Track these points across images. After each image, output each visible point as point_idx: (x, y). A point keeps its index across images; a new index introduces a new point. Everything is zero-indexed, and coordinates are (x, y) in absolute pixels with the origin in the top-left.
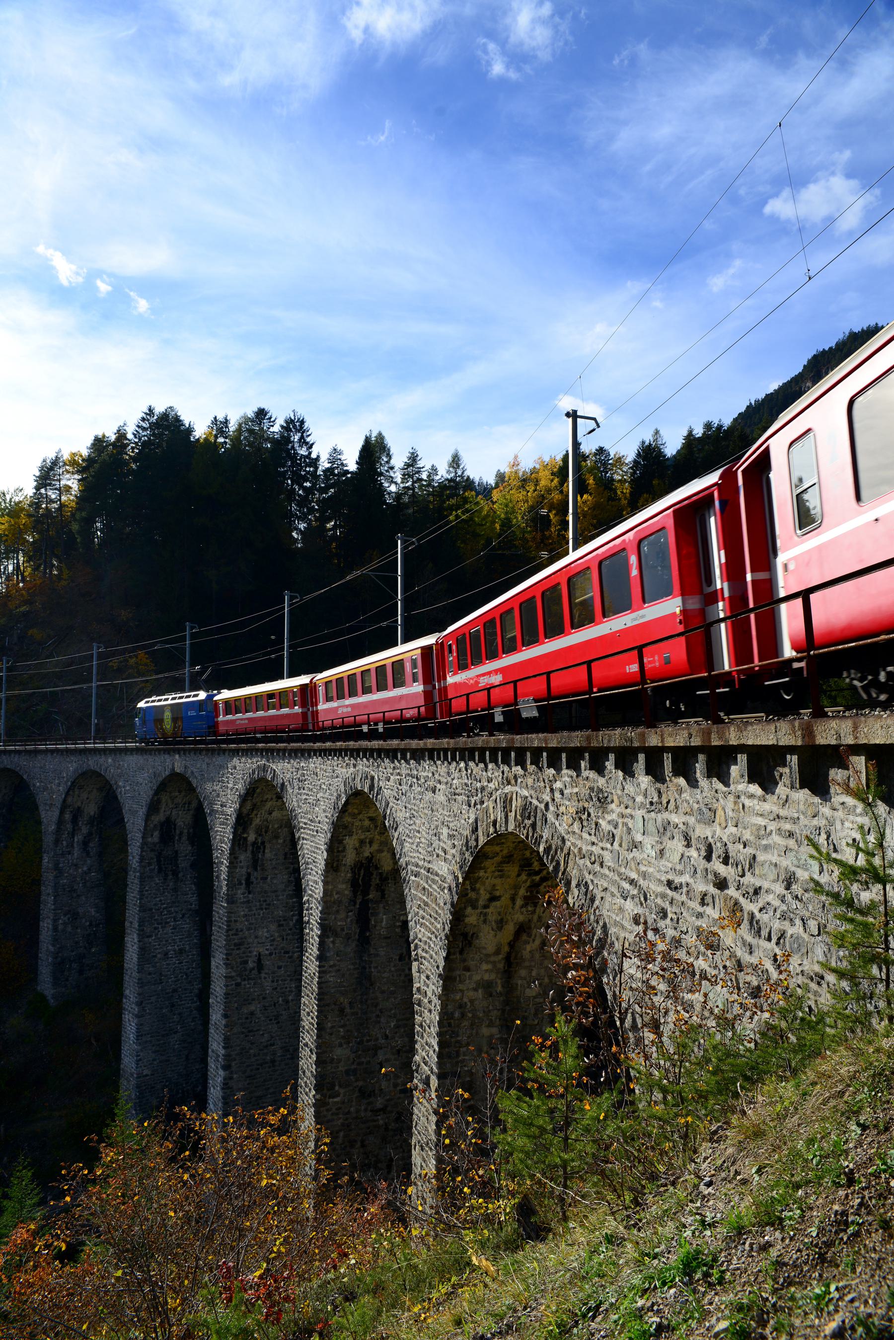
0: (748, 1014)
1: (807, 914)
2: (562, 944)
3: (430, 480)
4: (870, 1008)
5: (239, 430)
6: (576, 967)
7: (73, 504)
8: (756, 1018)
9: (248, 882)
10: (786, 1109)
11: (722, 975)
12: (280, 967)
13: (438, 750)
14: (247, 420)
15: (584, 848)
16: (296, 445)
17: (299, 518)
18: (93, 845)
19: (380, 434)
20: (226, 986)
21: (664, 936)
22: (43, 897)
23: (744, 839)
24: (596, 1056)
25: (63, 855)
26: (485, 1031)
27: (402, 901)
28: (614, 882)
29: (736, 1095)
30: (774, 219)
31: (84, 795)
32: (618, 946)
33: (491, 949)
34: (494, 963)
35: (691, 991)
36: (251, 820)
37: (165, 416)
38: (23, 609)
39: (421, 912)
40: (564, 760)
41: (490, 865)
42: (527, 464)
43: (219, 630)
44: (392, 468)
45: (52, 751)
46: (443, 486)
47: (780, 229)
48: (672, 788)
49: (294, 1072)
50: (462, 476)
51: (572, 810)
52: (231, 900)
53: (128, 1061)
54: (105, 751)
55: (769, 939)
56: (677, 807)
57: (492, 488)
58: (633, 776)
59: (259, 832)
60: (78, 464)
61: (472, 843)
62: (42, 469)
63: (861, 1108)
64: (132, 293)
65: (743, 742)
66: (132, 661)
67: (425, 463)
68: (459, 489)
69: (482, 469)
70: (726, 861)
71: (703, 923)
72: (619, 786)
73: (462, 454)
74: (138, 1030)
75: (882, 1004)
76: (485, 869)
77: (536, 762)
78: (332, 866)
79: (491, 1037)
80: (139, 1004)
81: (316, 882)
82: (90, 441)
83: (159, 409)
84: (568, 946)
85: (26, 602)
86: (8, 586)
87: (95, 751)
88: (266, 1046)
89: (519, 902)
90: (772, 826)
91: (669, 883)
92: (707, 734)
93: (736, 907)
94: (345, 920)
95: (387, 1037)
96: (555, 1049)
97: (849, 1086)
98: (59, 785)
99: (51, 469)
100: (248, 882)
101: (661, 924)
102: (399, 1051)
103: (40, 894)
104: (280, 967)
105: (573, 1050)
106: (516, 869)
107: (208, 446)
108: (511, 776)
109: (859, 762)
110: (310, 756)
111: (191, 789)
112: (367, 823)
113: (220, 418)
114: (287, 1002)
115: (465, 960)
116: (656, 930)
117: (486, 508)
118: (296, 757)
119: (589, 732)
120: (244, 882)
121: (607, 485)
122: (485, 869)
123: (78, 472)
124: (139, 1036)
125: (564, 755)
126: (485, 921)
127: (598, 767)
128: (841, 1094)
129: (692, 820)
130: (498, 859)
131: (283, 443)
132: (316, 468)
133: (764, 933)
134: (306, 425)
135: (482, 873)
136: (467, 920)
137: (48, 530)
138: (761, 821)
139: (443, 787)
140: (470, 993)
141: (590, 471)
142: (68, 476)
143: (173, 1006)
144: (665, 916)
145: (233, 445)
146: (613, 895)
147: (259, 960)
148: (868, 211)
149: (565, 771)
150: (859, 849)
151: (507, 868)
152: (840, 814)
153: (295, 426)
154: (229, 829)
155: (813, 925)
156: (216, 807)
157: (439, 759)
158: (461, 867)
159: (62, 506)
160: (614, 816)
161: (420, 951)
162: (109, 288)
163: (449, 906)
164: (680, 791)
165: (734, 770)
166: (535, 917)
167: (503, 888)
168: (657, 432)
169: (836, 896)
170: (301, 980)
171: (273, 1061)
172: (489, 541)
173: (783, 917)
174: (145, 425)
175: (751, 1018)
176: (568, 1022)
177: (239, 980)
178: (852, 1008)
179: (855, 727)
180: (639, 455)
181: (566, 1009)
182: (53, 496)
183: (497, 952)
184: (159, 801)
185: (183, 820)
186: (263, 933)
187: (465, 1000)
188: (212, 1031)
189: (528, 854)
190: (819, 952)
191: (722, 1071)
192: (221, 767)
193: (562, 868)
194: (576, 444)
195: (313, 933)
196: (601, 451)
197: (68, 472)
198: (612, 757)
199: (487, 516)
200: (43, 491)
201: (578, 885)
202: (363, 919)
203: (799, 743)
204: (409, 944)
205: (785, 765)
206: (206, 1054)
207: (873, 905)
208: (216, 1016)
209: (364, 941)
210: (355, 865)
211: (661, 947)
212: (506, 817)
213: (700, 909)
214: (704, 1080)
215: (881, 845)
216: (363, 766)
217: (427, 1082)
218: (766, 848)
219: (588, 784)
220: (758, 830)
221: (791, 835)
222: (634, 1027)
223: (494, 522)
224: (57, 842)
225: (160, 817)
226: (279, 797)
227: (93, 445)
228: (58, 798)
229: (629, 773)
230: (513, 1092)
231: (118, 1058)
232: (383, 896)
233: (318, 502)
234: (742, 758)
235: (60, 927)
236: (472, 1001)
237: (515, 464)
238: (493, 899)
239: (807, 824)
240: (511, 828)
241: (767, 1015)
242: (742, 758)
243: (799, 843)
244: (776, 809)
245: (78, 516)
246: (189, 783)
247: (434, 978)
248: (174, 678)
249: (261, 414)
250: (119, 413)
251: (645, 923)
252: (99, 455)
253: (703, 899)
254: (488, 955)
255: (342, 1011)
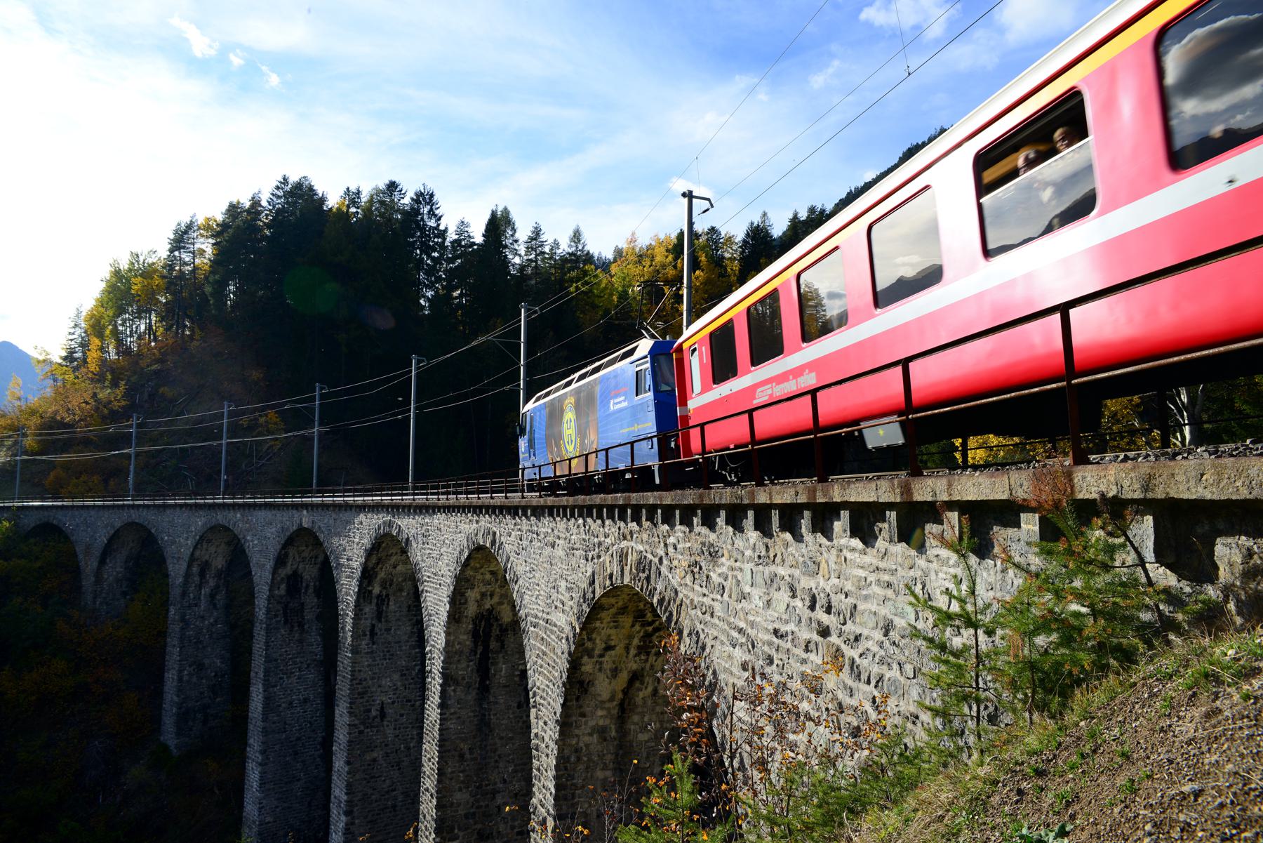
0: (849, 751)
1: (904, 659)
2: (677, 687)
3: (552, 254)
4: (961, 743)
5: (371, 201)
6: (691, 709)
7: (207, 267)
8: (856, 755)
9: (373, 633)
10: (890, 835)
11: (825, 717)
12: (402, 715)
13: (558, 507)
14: (378, 192)
15: (696, 599)
16: (426, 217)
17: (427, 286)
18: (221, 598)
19: (506, 209)
20: (350, 734)
21: (770, 682)
22: (169, 649)
23: (846, 590)
24: (709, 793)
25: (190, 607)
26: (600, 774)
27: (521, 651)
28: (723, 631)
29: (841, 824)
30: (868, 25)
31: (212, 549)
32: (728, 692)
33: (605, 695)
34: (608, 709)
35: (794, 732)
36: (376, 574)
37: (299, 186)
38: (154, 367)
39: (540, 661)
40: (678, 516)
41: (606, 616)
42: (643, 241)
43: (347, 392)
44: (516, 241)
45: (181, 506)
46: (564, 260)
47: (874, 35)
48: (779, 543)
49: (415, 816)
50: (582, 251)
51: (685, 564)
52: (355, 650)
53: (251, 809)
54: (234, 506)
55: (869, 682)
56: (783, 561)
57: (610, 263)
58: (742, 532)
59: (384, 585)
60: (212, 229)
61: (589, 595)
62: (176, 232)
63: (959, 830)
64: (264, 68)
65: (845, 499)
66: (262, 420)
67: (548, 237)
68: (579, 262)
69: (601, 246)
70: (828, 610)
71: (807, 669)
72: (729, 541)
73: (582, 229)
74: (261, 778)
75: (972, 740)
76: (601, 620)
77: (650, 518)
78: (455, 617)
79: (605, 779)
80: (263, 752)
81: (438, 633)
82: (225, 207)
83: (294, 178)
84: (682, 689)
85: (158, 361)
86: (139, 346)
87: (224, 506)
88: (388, 792)
89: (633, 651)
90: (872, 578)
91: (776, 632)
92: (812, 492)
93: (838, 653)
94: (466, 669)
95: (505, 781)
96: (672, 786)
97: (948, 811)
98: (187, 539)
99: (185, 232)
100: (373, 633)
101: (768, 670)
102: (516, 795)
103: (165, 645)
104: (402, 715)
105: (688, 787)
106: (630, 620)
107: (341, 216)
108: (627, 532)
109: (953, 516)
110: (434, 513)
111: (318, 544)
112: (488, 576)
113: (353, 189)
114: (409, 749)
115: (581, 707)
116: (763, 675)
117: (605, 281)
118: (421, 513)
119: (701, 490)
120: (368, 633)
121: (718, 262)
122: (601, 620)
123: (213, 236)
124: (263, 783)
125: (677, 512)
126: (600, 670)
127: (709, 523)
128: (942, 818)
129: (797, 573)
130: (613, 611)
131: (412, 215)
132: (444, 239)
133: (864, 677)
134: (435, 199)
135: (598, 624)
136: (583, 669)
137: (181, 292)
138: (862, 573)
139: (561, 542)
140: (585, 738)
141: (703, 248)
142: (202, 240)
143: (296, 753)
144: (771, 662)
145: (365, 215)
146: (722, 643)
147: (382, 708)
148: (951, 23)
149: (678, 527)
150: (951, 596)
151: (621, 619)
152: (934, 566)
153: (424, 199)
154: (355, 582)
155: (909, 669)
156: (342, 561)
157: (558, 515)
158: (578, 618)
159: (195, 269)
160: (724, 569)
161: (538, 698)
162: (242, 62)
163: (566, 655)
164: (787, 546)
165: (837, 526)
166: (648, 666)
167: (617, 637)
168: (765, 214)
169: (931, 641)
170: (422, 727)
171: (394, 806)
172: (607, 312)
173: (881, 662)
174: (280, 193)
175: (852, 755)
176: (684, 761)
177: (362, 728)
178: (948, 744)
179: (950, 485)
180: (748, 235)
181: (682, 749)
182: (187, 259)
183: (612, 699)
184: (286, 555)
185: (310, 573)
186: (386, 682)
187: (581, 744)
188: (335, 777)
189: (641, 605)
190: (915, 693)
191: (828, 804)
192: (348, 522)
193: (674, 618)
194: (691, 224)
195: (435, 683)
196: (713, 230)
197: (202, 236)
198: (723, 513)
199: (606, 288)
200: (177, 253)
201: (690, 635)
202: (483, 670)
203: (898, 500)
204: (527, 692)
205: (884, 521)
206: (329, 801)
207: (966, 648)
208: (339, 763)
209: (484, 690)
210: (477, 617)
211: (769, 690)
212: (622, 571)
213: (804, 656)
214: (810, 812)
215: (973, 593)
216: (486, 522)
217: (543, 823)
218: (866, 598)
219: (700, 539)
220: (859, 581)
221: (889, 585)
222: (742, 767)
223: (612, 295)
224: (184, 594)
225: (288, 570)
226: (404, 551)
227: (228, 210)
228: (186, 552)
229: (739, 528)
230: (632, 827)
231: (241, 806)
232: (503, 646)
233: (445, 271)
234: (845, 515)
235: (185, 678)
236: (587, 746)
237: (633, 240)
238: (609, 648)
239: (904, 574)
240: (626, 581)
241: (866, 752)
242: (845, 515)
243: (897, 593)
244: (875, 562)
245: (211, 279)
246: (316, 538)
247: (551, 724)
248: (303, 436)
249: (392, 186)
250: (254, 181)
251: (753, 669)
252: (233, 221)
253: (807, 646)
254: (603, 702)
255: (462, 756)
